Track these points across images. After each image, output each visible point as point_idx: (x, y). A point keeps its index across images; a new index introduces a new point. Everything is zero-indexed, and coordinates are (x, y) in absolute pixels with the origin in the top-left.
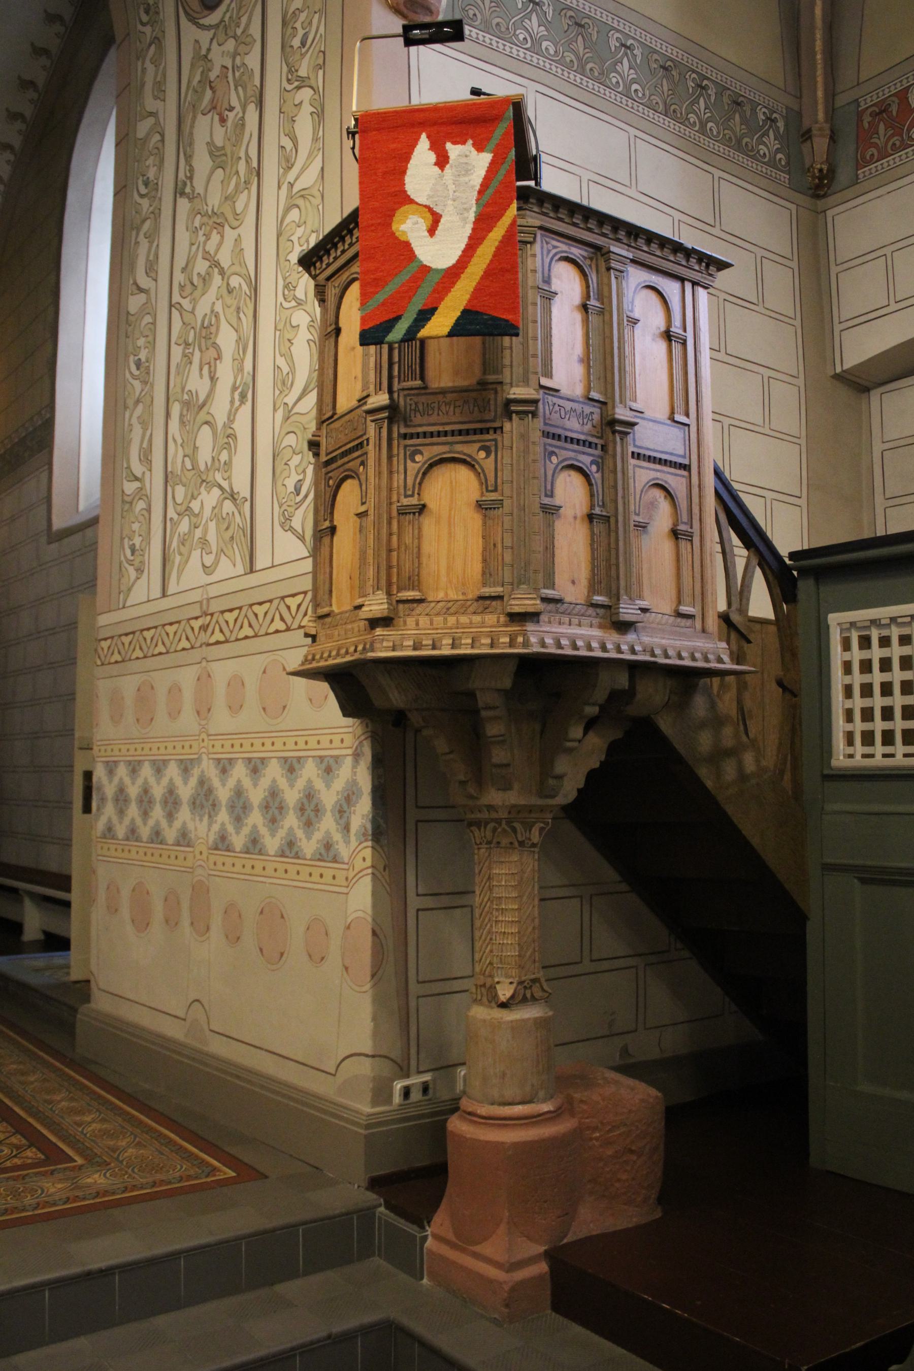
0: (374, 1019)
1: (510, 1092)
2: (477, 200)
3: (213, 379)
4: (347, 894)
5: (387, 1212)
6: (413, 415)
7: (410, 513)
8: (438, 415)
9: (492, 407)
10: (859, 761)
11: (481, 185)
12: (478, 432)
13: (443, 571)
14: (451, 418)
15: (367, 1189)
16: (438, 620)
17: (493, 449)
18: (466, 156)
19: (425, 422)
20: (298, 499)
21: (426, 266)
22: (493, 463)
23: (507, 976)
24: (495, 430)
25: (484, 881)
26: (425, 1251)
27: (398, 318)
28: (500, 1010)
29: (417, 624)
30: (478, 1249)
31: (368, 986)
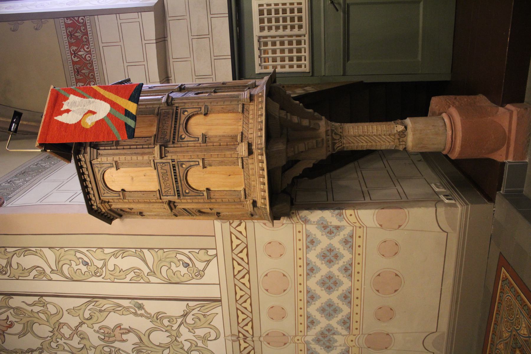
0: (420, 207)
1: (441, 124)
2: (87, 98)
3: (129, 331)
4: (367, 227)
5: (502, 189)
6: (166, 139)
7: (205, 139)
8: (167, 130)
9: (168, 110)
10: (307, 63)
11: (82, 97)
12: (176, 115)
13: (232, 127)
14: (169, 124)
15: (494, 202)
16: (250, 126)
17: (184, 109)
18: (69, 103)
19: (169, 134)
20: (191, 265)
21: (107, 115)
22: (190, 109)
23: (394, 128)
24: (177, 109)
25: (356, 140)
26: (514, 161)
27: (126, 124)
28: (408, 129)
29: (252, 134)
30: (507, 130)
31: (406, 210)
